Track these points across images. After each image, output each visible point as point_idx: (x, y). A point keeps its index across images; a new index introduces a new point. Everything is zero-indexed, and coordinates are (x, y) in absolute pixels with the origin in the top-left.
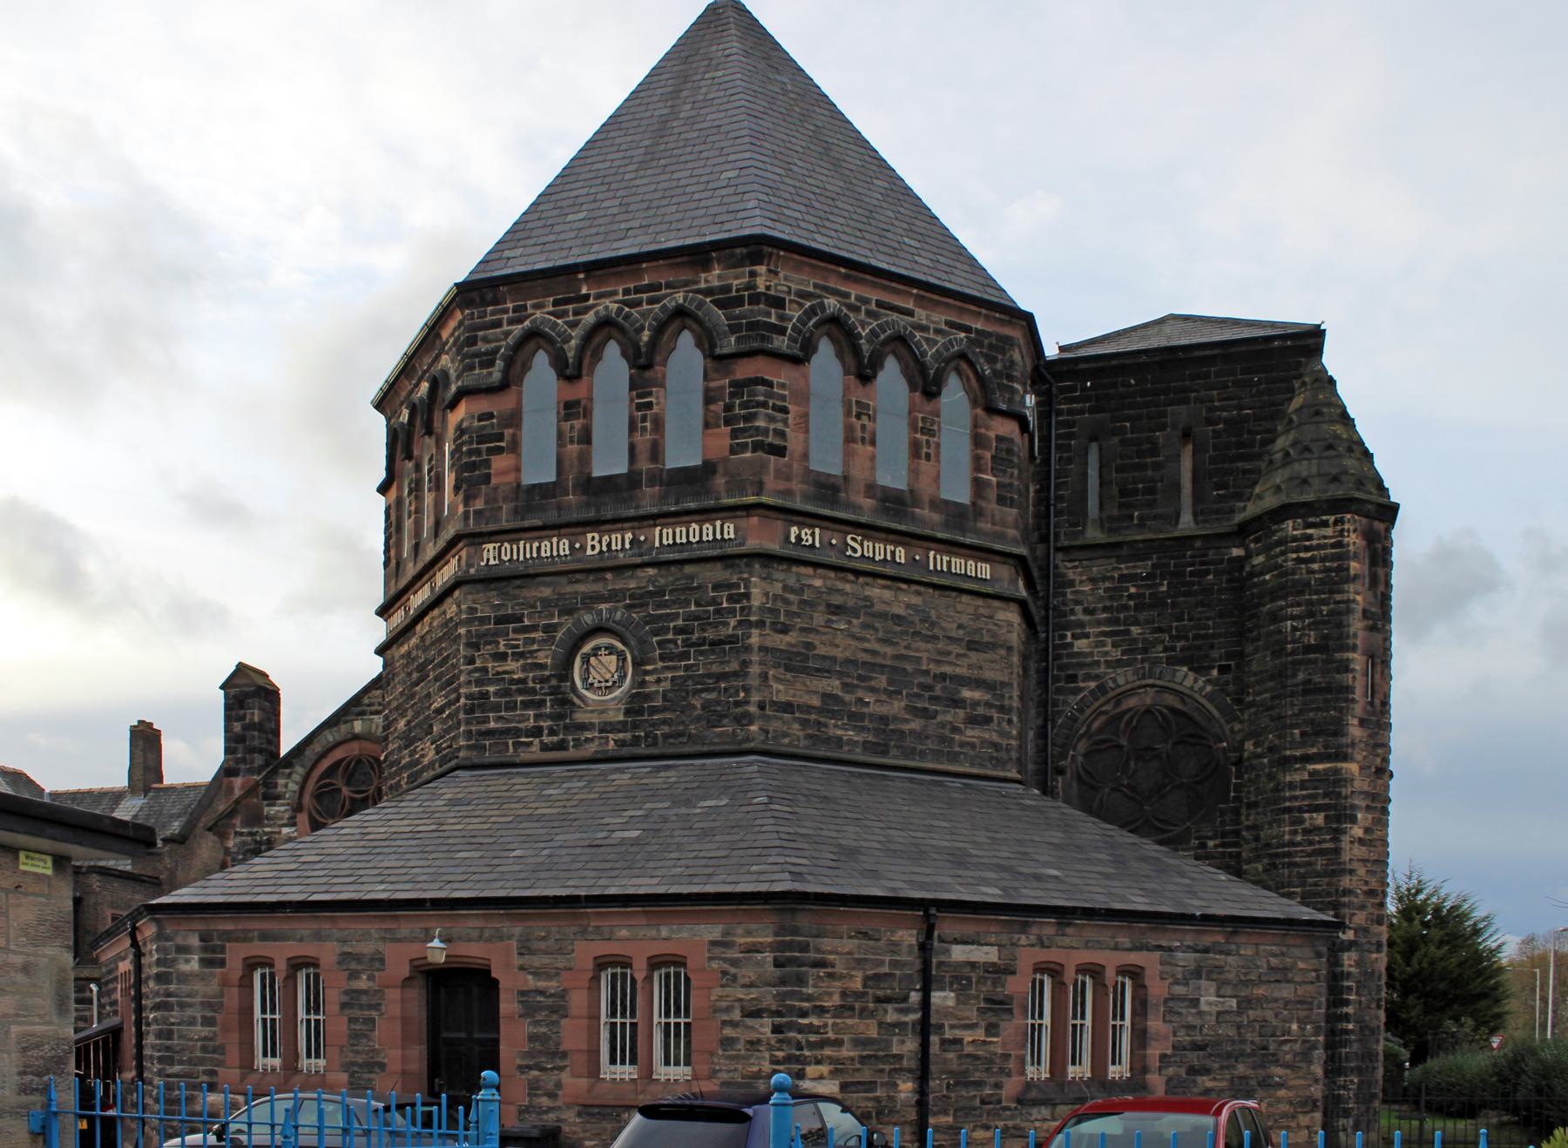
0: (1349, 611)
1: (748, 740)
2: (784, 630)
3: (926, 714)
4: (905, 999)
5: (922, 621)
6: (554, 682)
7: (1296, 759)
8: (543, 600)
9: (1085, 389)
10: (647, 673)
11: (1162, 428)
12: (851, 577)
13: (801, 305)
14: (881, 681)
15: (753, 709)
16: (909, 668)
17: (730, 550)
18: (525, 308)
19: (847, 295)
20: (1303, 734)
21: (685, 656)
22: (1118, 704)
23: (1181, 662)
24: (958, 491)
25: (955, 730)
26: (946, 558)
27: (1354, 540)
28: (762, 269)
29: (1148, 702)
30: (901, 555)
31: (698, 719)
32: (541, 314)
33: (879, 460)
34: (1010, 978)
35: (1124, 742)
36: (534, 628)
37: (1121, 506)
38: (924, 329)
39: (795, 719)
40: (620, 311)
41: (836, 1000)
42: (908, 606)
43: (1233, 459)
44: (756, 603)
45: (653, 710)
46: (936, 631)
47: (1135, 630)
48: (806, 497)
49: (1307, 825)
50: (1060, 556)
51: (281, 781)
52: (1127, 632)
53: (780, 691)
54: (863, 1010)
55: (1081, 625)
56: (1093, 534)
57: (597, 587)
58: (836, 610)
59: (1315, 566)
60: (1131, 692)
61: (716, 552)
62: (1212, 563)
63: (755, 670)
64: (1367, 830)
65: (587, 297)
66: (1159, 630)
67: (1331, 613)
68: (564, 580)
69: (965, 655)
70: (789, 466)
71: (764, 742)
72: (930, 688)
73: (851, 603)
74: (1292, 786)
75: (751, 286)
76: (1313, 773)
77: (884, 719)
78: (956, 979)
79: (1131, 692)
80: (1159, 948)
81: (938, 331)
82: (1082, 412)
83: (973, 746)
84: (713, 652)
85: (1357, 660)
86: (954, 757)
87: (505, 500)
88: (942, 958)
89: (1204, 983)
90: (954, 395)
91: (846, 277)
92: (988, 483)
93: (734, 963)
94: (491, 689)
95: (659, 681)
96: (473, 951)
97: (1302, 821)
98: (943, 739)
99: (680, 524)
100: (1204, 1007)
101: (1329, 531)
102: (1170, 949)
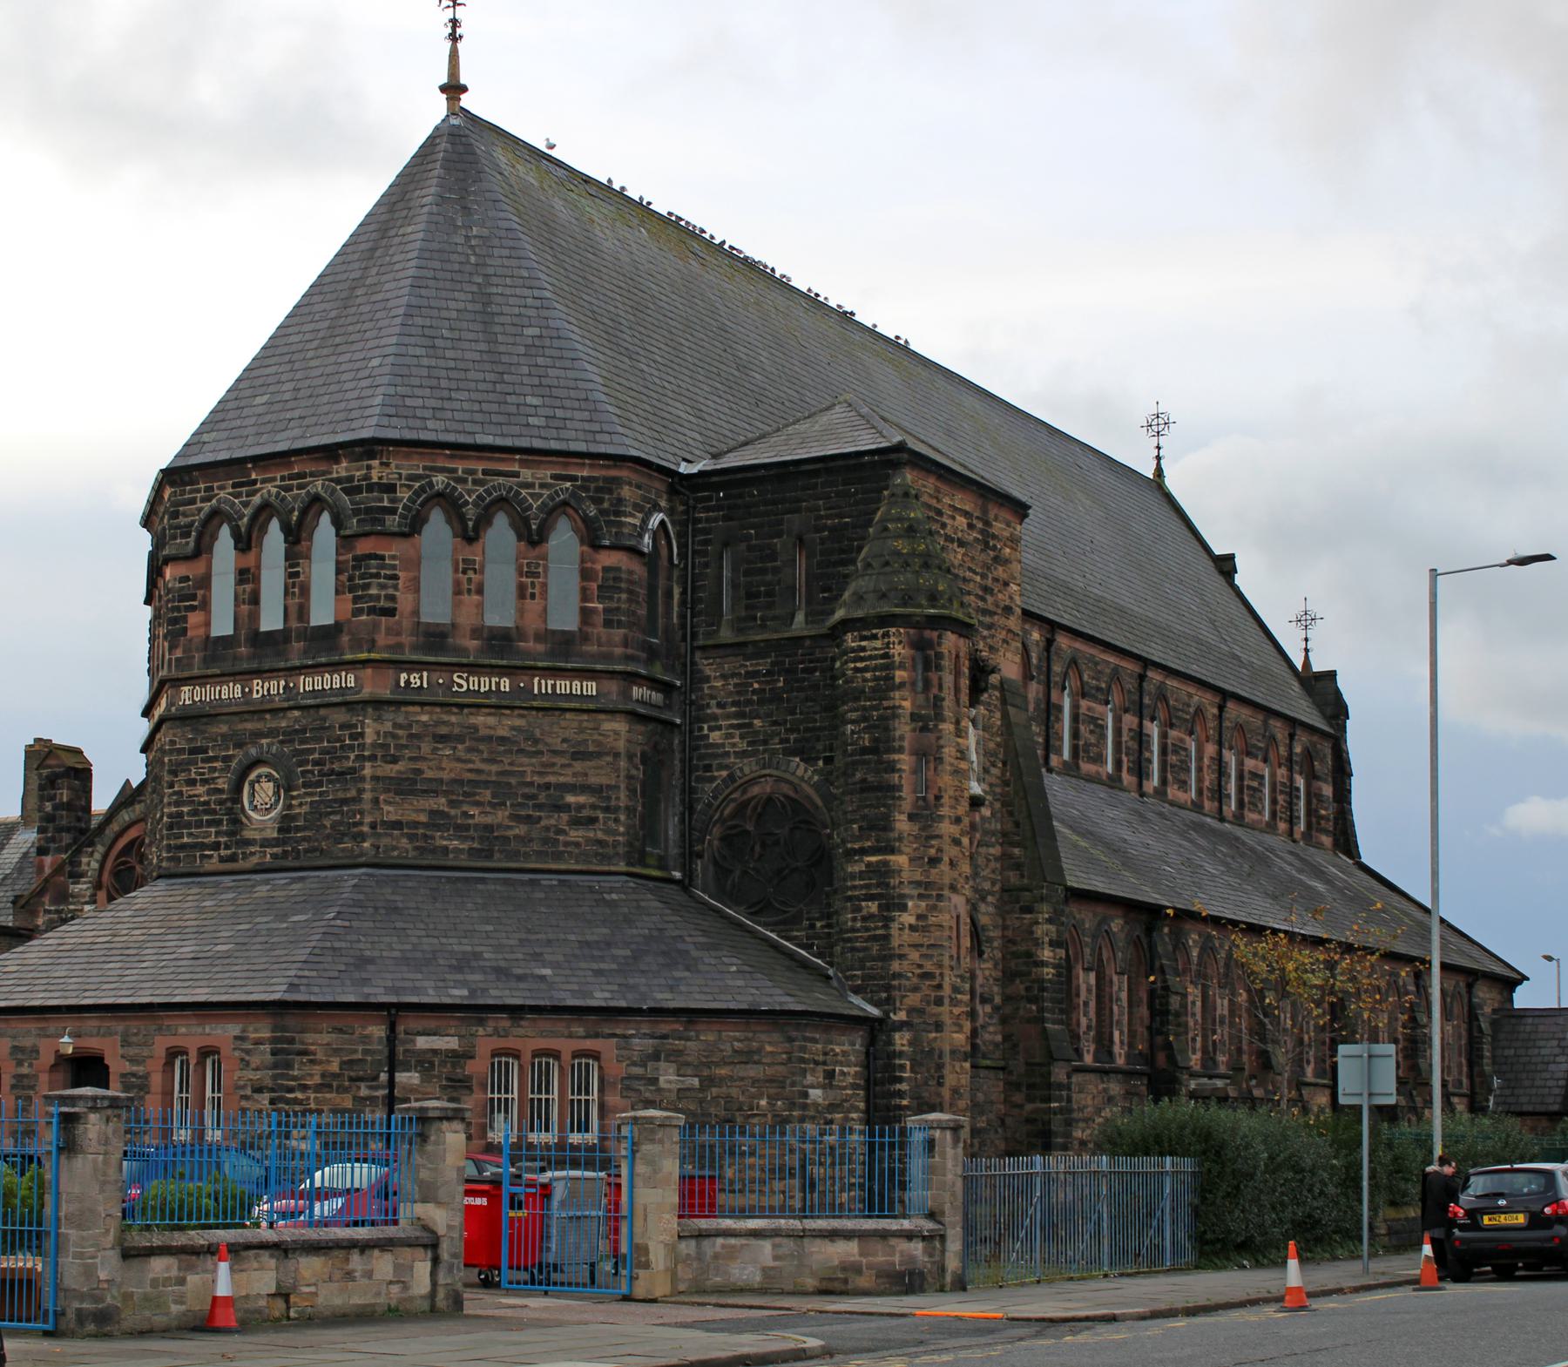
0: (895, 716)
1: (361, 855)
2: (394, 760)
3: (528, 819)
4: (376, 1078)
5: (526, 739)
6: (229, 804)
7: (855, 852)
8: (223, 736)
9: (719, 499)
10: (293, 798)
11: (779, 535)
12: (455, 710)
13: (410, 487)
14: (487, 795)
15: (366, 829)
16: (513, 781)
17: (349, 698)
18: (212, 488)
19: (455, 470)
20: (860, 828)
21: (319, 784)
22: (744, 792)
23: (793, 753)
24: (565, 619)
25: (560, 832)
26: (550, 682)
27: (899, 651)
28: (375, 463)
29: (768, 790)
30: (505, 685)
31: (328, 837)
32: (224, 493)
33: (487, 605)
34: (469, 1062)
35: (750, 827)
36: (215, 759)
37: (747, 607)
38: (531, 485)
39: (402, 835)
40: (278, 494)
41: (317, 1080)
42: (513, 728)
43: (836, 564)
44: (368, 740)
45: (298, 829)
46: (540, 747)
47: (757, 722)
48: (415, 648)
49: (864, 912)
50: (698, 654)
51: (85, 860)
52: (750, 725)
53: (390, 812)
54: (338, 1087)
55: (715, 718)
56: (726, 635)
57: (259, 725)
58: (442, 739)
59: (868, 675)
60: (753, 781)
61: (339, 699)
62: (818, 661)
63: (367, 796)
64: (920, 917)
65: (254, 482)
66: (775, 723)
67: (881, 718)
68: (235, 718)
69: (569, 765)
70: (399, 623)
71: (376, 856)
72: (534, 797)
73: (456, 731)
74: (853, 876)
75: (367, 477)
76: (869, 864)
77: (489, 828)
78: (420, 1063)
79: (753, 781)
80: (614, 1035)
81: (542, 486)
82: (716, 520)
83: (577, 844)
84: (338, 781)
85: (905, 761)
86: (558, 856)
87: (197, 650)
88: (408, 1047)
89: (662, 1064)
90: (564, 540)
91: (451, 457)
92: (594, 610)
93: (248, 1052)
94: (185, 809)
95: (301, 805)
96: (93, 1043)
97: (859, 909)
98: (545, 841)
99: (318, 673)
100: (662, 1083)
101: (878, 644)
102: (625, 1036)
